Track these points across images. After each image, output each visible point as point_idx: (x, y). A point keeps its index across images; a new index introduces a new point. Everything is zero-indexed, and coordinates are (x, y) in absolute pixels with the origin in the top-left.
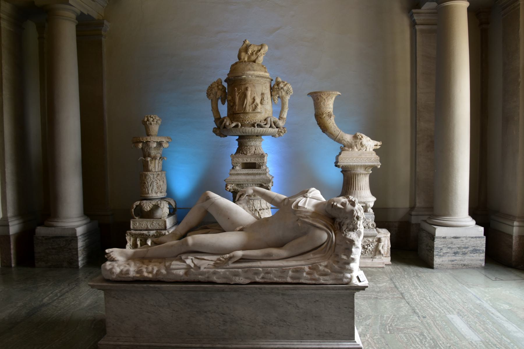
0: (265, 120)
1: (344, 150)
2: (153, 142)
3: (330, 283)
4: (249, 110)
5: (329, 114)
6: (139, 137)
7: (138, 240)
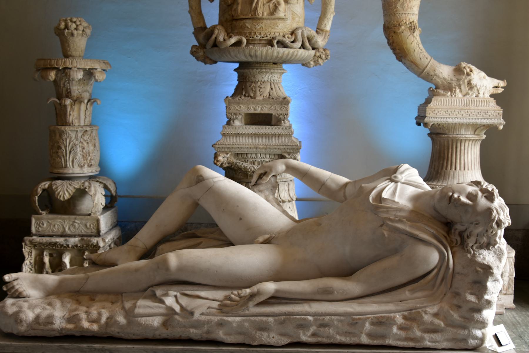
0: (292, 33)
1: (438, 95)
2: (76, 69)
3: (443, 347)
4: (263, 13)
5: (411, 26)
6: (50, 60)
7: (46, 256)
